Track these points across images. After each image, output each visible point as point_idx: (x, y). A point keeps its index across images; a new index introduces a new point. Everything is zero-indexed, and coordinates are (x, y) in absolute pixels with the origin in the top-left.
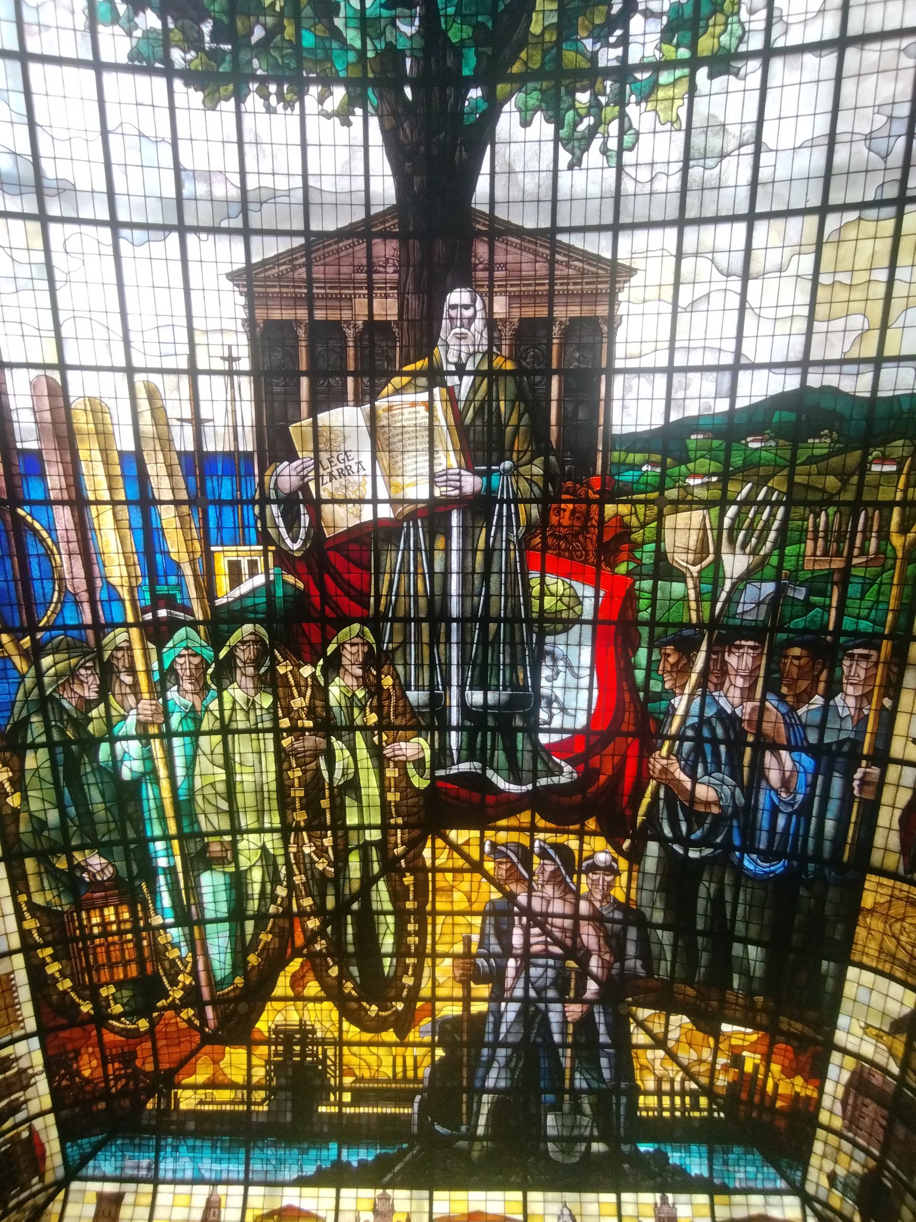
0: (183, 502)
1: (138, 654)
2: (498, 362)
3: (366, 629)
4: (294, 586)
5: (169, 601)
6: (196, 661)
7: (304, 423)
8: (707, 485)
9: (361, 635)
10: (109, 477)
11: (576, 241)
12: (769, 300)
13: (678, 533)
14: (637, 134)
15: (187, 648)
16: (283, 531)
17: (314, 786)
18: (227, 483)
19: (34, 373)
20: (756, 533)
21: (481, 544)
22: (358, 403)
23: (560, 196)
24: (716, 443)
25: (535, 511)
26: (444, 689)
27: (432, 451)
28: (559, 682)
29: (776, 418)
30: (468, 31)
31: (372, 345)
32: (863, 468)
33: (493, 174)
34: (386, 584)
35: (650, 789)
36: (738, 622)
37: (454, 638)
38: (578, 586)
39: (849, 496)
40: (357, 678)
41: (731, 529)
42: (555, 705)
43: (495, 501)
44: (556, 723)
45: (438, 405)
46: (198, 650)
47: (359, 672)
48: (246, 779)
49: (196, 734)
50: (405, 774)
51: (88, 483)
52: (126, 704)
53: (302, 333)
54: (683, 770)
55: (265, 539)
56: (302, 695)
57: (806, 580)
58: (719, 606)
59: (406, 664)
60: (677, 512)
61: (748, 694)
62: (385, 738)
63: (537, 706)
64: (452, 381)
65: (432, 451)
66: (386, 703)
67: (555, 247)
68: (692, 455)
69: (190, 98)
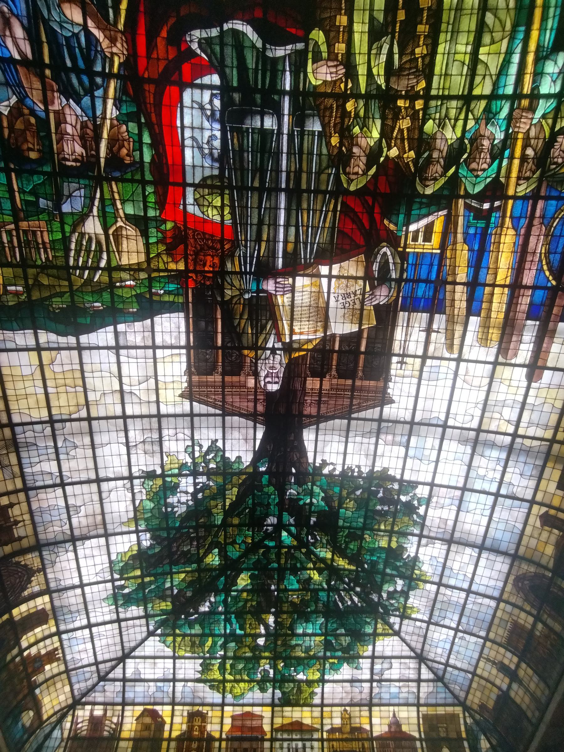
0: (450, 283)
1: (514, 174)
2: (252, 354)
3: (345, 186)
4: (390, 222)
5: (479, 215)
6: (474, 165)
7: (366, 326)
8: (122, 281)
9: (350, 181)
10: (491, 302)
11: (212, 410)
12: (107, 381)
13: (135, 249)
14: (186, 452)
15: (477, 176)
16: (391, 260)
17: (407, 38)
18: (420, 293)
19: (513, 361)
20: (84, 248)
21: (263, 245)
22: (334, 336)
23: (221, 429)
24: (121, 306)
25: (229, 266)
26: (293, 131)
27: (292, 306)
28: (207, 134)
29: (88, 320)
30: (266, 490)
31: (322, 366)
32: (28, 289)
33: (255, 439)
34: (328, 220)
35: (122, 20)
36: (82, 182)
37: (284, 175)
38: (198, 213)
39: (31, 272)
40: (357, 145)
41: (101, 251)
42: (209, 113)
43: (254, 274)
44: (207, 95)
45: (287, 332)
46: (470, 174)
47: (355, 150)
48: (463, 47)
49: (493, 97)
50: (330, 45)
51: (505, 299)
52: (538, 128)
53: (360, 374)
54: (98, 40)
55: (404, 256)
56: (401, 131)
57: (41, 213)
58: (98, 195)
59: (320, 155)
60: (138, 264)
61: (60, 119)
62: (342, 86)
63: (222, 111)
64: (278, 345)
65: (292, 306)
66: (338, 120)
67: (223, 408)
68: (134, 299)
69: (395, 473)
